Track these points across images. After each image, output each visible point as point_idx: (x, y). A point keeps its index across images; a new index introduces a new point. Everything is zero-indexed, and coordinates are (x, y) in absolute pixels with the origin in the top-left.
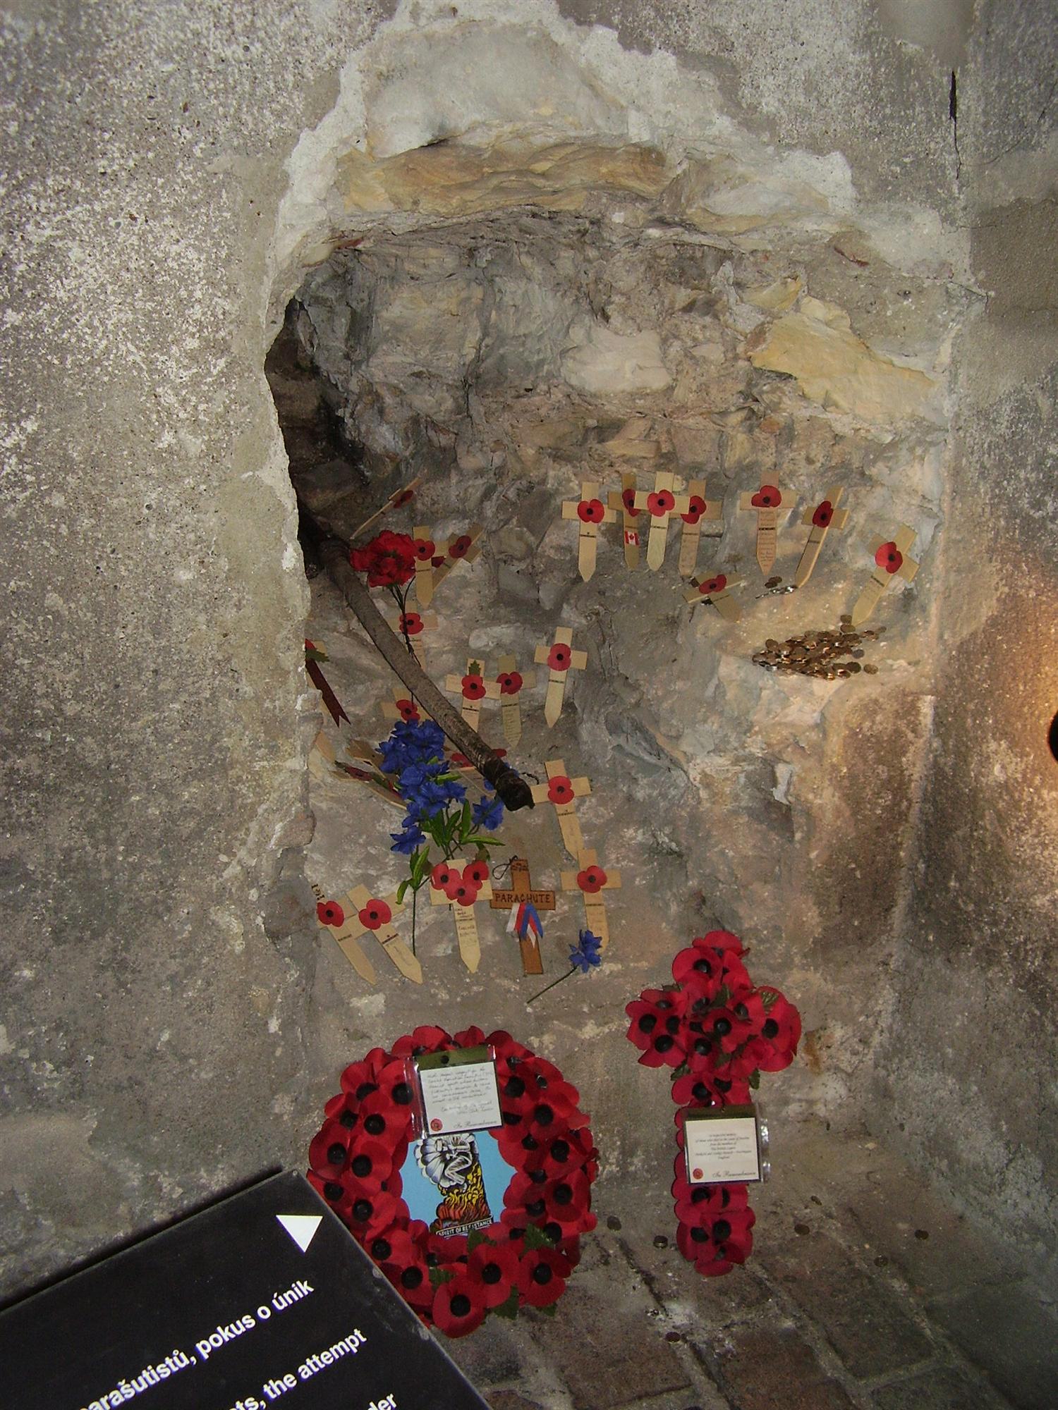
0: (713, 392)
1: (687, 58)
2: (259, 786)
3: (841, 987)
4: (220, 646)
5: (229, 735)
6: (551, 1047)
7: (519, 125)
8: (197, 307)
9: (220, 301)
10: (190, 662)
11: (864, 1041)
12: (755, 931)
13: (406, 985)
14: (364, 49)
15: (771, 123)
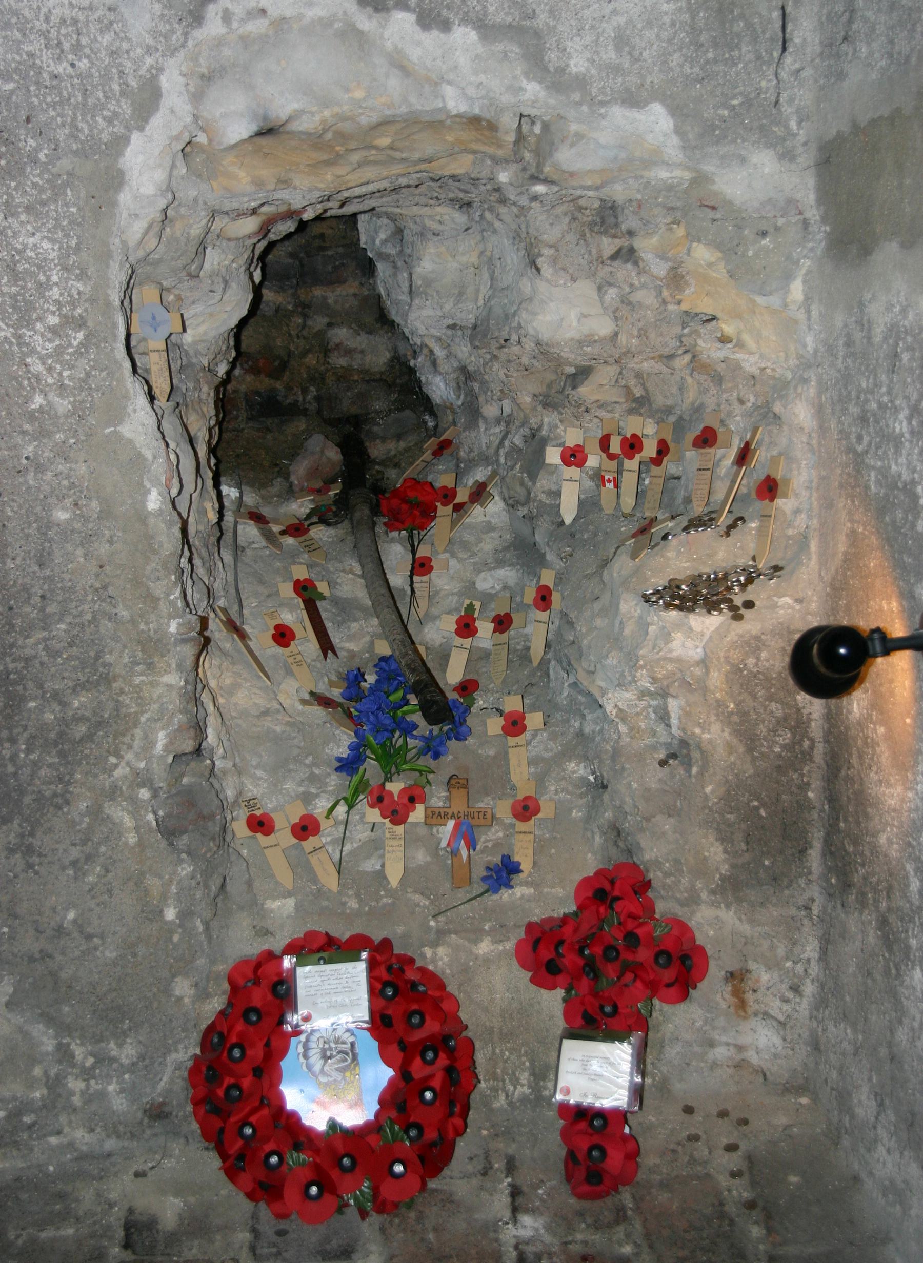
0: (652, 336)
1: (486, 29)
2: (140, 697)
3: (759, 929)
4: (97, 575)
5: (111, 653)
6: (446, 959)
7: (337, 109)
8: (55, 289)
9: (74, 283)
10: (72, 589)
11: (796, 989)
12: (658, 864)
13: (320, 893)
14: (181, 55)
15: (581, 82)
